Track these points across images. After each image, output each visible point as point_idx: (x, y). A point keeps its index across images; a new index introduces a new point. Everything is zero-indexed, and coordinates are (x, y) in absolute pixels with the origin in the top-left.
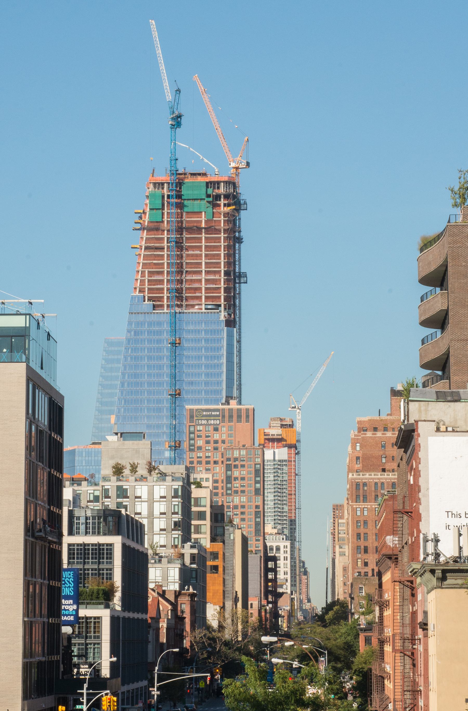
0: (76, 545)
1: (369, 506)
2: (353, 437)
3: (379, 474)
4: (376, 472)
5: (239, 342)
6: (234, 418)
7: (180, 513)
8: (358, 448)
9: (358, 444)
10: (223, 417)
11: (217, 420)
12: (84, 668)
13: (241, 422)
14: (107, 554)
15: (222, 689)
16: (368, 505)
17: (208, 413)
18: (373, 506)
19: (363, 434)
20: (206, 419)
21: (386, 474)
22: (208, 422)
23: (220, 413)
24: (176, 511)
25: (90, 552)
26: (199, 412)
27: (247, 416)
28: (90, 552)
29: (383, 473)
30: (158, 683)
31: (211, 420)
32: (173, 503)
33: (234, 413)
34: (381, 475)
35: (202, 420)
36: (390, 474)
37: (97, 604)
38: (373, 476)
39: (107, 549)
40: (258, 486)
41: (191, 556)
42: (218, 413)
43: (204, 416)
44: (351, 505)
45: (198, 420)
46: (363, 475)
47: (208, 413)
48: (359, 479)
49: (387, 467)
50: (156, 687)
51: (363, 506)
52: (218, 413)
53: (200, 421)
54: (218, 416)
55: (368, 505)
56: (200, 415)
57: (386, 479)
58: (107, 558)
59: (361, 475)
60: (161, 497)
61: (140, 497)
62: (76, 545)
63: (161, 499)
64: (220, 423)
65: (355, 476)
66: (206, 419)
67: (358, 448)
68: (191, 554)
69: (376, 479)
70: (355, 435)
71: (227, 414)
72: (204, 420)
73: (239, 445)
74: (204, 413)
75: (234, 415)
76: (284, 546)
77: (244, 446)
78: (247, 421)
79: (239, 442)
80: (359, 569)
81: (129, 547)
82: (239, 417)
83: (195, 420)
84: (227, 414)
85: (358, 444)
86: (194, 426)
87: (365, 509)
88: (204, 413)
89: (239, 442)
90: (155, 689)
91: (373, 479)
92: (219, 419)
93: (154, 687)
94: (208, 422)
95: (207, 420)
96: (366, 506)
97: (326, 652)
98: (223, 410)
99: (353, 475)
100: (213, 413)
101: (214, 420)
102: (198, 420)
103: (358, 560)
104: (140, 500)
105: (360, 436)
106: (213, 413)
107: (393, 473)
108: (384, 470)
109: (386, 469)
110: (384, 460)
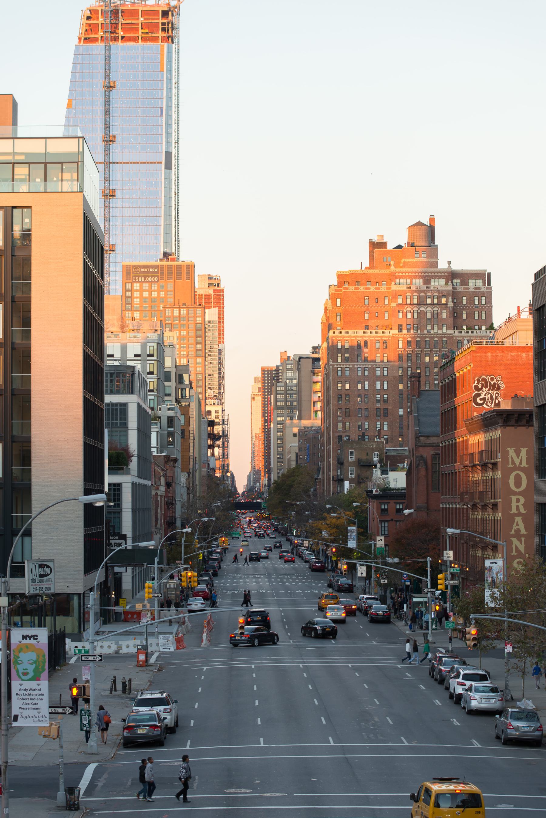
0: (119, 405)
1: (351, 366)
2: (334, 292)
3: (362, 331)
4: (358, 329)
5: (177, 194)
6: (173, 275)
7: (155, 372)
8: (339, 304)
9: (339, 300)
10: (162, 273)
11: (155, 277)
12: (114, 539)
13: (181, 279)
14: (121, 414)
15: (441, 573)
16: (369, 365)
17: (146, 270)
18: (356, 366)
19: (345, 288)
20: (143, 276)
21: (369, 331)
22: (145, 279)
23: (158, 270)
24: (152, 370)
25: (119, 412)
26: (136, 268)
27: (188, 273)
28: (119, 412)
29: (366, 330)
30: (184, 556)
31: (149, 277)
32: (149, 362)
33: (173, 270)
34: (364, 333)
35: (139, 277)
36: (374, 331)
37: (117, 470)
38: (355, 334)
39: (121, 409)
40: (199, 347)
41: (168, 419)
42: (156, 270)
43: (141, 273)
44: (331, 365)
45: (135, 277)
46: (345, 333)
47: (146, 270)
48: (341, 337)
49: (370, 324)
50: (183, 559)
51: (345, 366)
52: (156, 270)
53: (137, 278)
54: (157, 272)
55: (369, 365)
56: (138, 271)
57: (370, 337)
58: (121, 419)
59: (343, 333)
60: (136, 356)
61: (112, 356)
62: (119, 405)
63: (135, 358)
64: (158, 281)
65: (336, 334)
66: (143, 276)
67: (339, 304)
68: (168, 417)
69: (358, 337)
70: (335, 290)
71: (166, 271)
72: (141, 277)
73: (179, 304)
74: (142, 270)
75: (173, 271)
76: (216, 411)
77: (184, 304)
78: (188, 278)
79: (179, 300)
80: (340, 432)
81: (141, 406)
82: (179, 274)
83: (131, 277)
84: (166, 271)
85: (339, 300)
86: (131, 283)
87: (346, 369)
88: (142, 270)
89: (179, 300)
90: (182, 562)
91: (356, 337)
92: (158, 276)
93: (181, 560)
94: (145, 279)
95: (145, 277)
96: (348, 366)
97: (357, 521)
98: (162, 266)
99: (334, 333)
100: (151, 270)
101: (152, 277)
102: (135, 277)
103: (339, 424)
104: (112, 358)
105: (341, 290)
106: (151, 270)
107: (377, 331)
108: (367, 328)
109: (370, 327)
110: (367, 317)
